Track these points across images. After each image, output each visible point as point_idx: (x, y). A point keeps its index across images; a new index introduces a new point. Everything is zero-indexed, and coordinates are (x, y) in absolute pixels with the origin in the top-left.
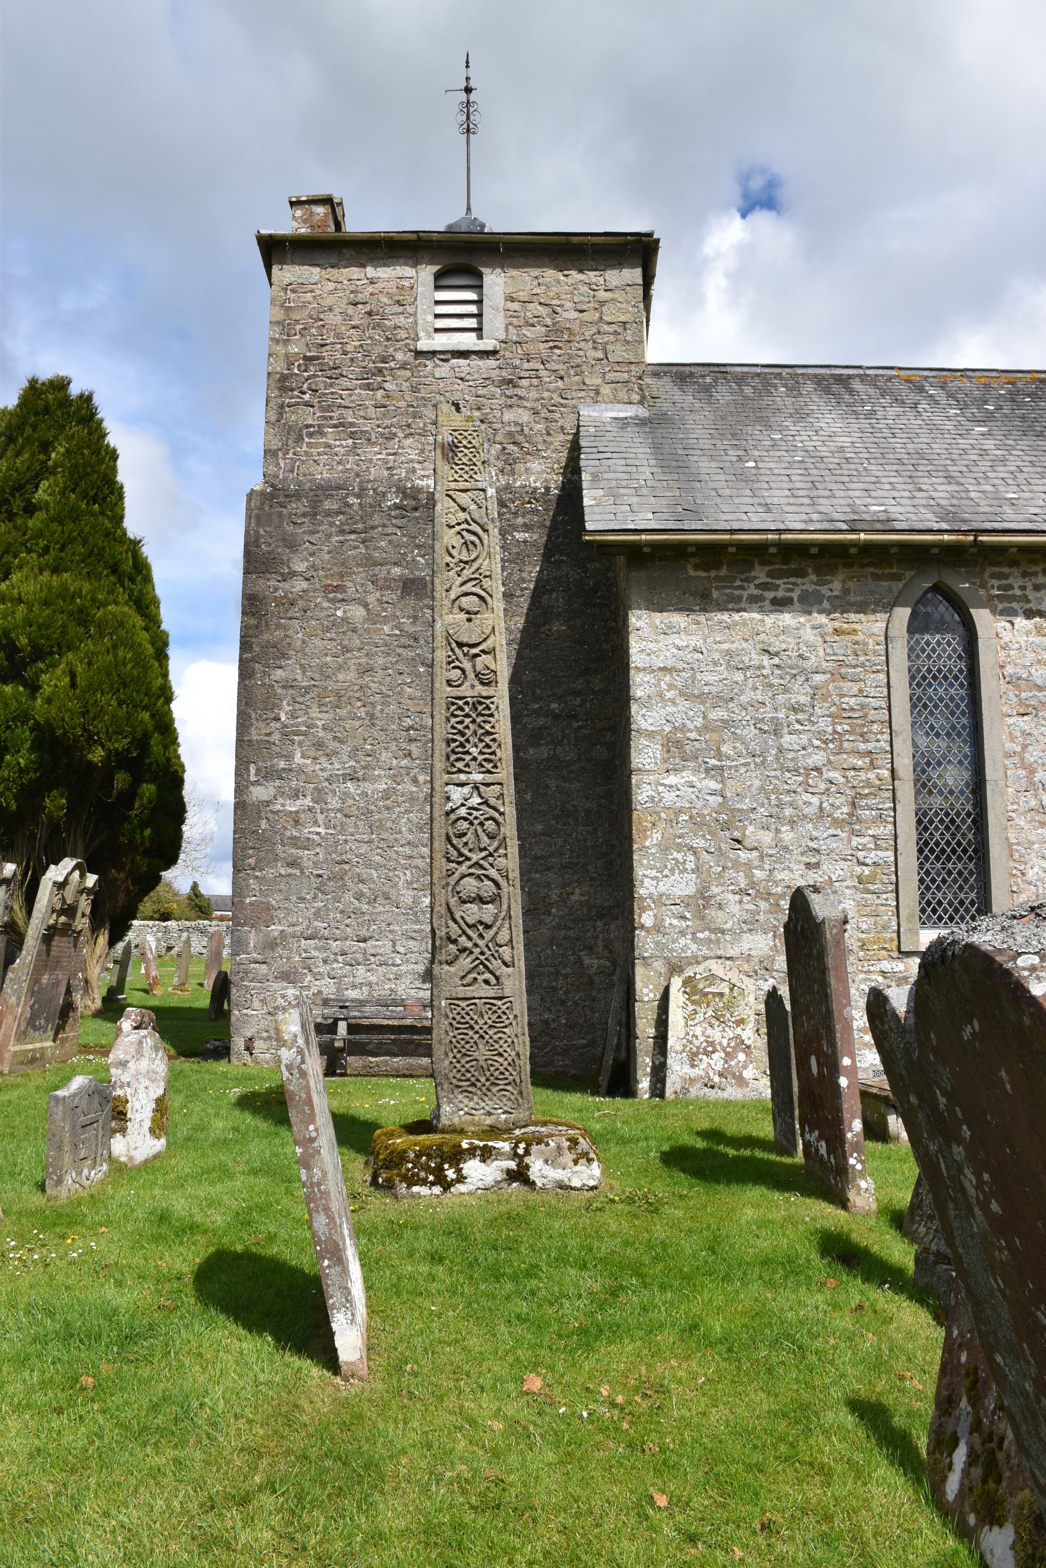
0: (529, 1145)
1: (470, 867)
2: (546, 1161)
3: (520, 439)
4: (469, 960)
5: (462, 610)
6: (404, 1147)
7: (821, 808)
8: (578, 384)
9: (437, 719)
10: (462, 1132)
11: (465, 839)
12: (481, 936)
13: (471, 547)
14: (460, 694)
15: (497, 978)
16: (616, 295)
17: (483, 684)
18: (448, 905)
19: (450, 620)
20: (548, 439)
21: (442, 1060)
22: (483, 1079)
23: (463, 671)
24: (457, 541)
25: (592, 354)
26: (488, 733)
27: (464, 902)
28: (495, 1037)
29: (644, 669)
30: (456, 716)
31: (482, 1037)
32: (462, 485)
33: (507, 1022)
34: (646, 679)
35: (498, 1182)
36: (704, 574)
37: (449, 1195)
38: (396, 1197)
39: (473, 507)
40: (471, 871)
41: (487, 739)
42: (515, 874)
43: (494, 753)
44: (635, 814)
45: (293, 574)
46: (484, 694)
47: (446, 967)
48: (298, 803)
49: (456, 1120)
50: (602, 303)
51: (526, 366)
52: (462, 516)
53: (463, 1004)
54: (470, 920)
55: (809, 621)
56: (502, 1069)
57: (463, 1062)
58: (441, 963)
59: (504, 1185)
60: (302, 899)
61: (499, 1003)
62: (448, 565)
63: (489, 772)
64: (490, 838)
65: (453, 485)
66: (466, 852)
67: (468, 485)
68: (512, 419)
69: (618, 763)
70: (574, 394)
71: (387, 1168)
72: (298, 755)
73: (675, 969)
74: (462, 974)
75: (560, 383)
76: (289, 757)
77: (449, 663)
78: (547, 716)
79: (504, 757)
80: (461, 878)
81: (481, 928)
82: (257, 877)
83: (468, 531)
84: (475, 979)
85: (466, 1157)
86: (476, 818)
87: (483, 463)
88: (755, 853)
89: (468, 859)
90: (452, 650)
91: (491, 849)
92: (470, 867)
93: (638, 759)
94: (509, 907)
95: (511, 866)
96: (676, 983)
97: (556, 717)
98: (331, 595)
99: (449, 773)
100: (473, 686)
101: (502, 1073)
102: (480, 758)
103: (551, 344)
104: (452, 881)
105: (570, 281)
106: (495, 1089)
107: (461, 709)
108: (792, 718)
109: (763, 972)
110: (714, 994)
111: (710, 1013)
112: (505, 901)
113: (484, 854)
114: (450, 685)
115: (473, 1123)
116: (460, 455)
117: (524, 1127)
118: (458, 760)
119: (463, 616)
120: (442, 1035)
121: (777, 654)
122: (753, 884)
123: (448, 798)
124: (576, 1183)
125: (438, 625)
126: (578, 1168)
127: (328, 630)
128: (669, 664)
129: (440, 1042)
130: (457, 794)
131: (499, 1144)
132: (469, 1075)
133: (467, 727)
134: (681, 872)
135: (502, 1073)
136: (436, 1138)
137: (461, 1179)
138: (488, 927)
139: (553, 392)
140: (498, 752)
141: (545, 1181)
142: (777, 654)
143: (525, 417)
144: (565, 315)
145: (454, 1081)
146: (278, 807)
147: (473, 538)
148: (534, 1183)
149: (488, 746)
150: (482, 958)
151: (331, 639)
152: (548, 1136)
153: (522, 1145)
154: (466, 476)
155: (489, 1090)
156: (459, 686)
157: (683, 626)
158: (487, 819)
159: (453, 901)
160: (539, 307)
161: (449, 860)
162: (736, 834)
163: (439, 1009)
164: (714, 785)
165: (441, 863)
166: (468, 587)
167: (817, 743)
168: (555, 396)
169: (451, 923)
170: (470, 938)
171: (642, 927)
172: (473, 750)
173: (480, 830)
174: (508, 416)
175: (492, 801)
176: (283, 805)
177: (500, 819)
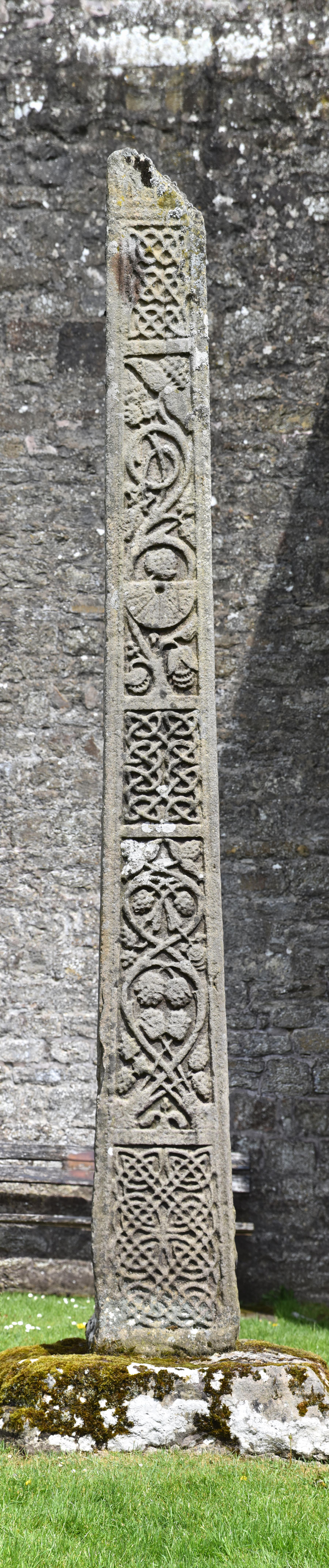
0: (228, 1376)
1: (154, 957)
2: (256, 1405)
4: (150, 1089)
5: (149, 573)
6: (42, 1368)
9: (111, 740)
10: (131, 1353)
11: (147, 917)
12: (167, 1055)
13: (165, 463)
14: (144, 706)
15: (189, 1117)
17: (178, 689)
18: (121, 1009)
19: (131, 589)
21: (107, 1238)
22: (165, 1271)
23: (150, 671)
24: (143, 454)
26: (184, 764)
27: (145, 1006)
28: (185, 1206)
30: (139, 738)
31: (165, 1205)
32: (153, 346)
33: (202, 1184)
34: (27, 1054)
35: (181, 1436)
37: (104, 1452)
38: (23, 1453)
39: (170, 388)
40: (156, 962)
41: (183, 773)
42: (217, 968)
43: (191, 794)
46: (180, 705)
47: (117, 1099)
49: (123, 1334)
52: (152, 405)
53: (139, 1154)
54: (153, 1033)
56: (193, 1255)
57: (136, 1241)
58: (109, 1093)
59: (190, 1441)
61: (191, 1154)
62: (128, 495)
63: (184, 821)
64: (183, 916)
65: (137, 346)
66: (148, 934)
67: (160, 346)
71: (13, 1403)
77: (130, 658)
79: (205, 800)
80: (142, 972)
81: (167, 1043)
83: (161, 433)
84: (157, 1118)
85: (134, 1389)
86: (164, 887)
87: (190, 297)
89: (152, 945)
90: (134, 638)
91: (184, 931)
92: (154, 957)
94: (208, 1015)
95: (211, 956)
99: (127, 822)
100: (163, 694)
101: (193, 1262)
102: (172, 800)
104: (129, 975)
106: (182, 1287)
112: (202, 1005)
113: (174, 938)
114: (130, 692)
115: (148, 1340)
116: (149, 281)
117: (226, 1350)
119: (151, 583)
120: (106, 1199)
123: (125, 859)
124: (304, 1446)
125: (113, 598)
126: (305, 1420)
129: (104, 1210)
130: (138, 853)
131: (184, 1373)
132: (144, 1263)
133: (154, 755)
135: (193, 1262)
136: (91, 1359)
137: (124, 1426)
138: (177, 1042)
140: (197, 791)
141: (254, 1439)
145: (123, 1271)
147: (169, 447)
148: (236, 1442)
149: (183, 783)
150: (168, 1087)
152: (259, 1365)
153: (219, 1376)
154: (159, 327)
155: (173, 1287)
156: (144, 693)
158: (179, 889)
159: (129, 1005)
161: (124, 946)
163: (105, 1159)
165: (114, 951)
169: (125, 1036)
170: (151, 1058)
175: (188, 864)
177: (198, 889)
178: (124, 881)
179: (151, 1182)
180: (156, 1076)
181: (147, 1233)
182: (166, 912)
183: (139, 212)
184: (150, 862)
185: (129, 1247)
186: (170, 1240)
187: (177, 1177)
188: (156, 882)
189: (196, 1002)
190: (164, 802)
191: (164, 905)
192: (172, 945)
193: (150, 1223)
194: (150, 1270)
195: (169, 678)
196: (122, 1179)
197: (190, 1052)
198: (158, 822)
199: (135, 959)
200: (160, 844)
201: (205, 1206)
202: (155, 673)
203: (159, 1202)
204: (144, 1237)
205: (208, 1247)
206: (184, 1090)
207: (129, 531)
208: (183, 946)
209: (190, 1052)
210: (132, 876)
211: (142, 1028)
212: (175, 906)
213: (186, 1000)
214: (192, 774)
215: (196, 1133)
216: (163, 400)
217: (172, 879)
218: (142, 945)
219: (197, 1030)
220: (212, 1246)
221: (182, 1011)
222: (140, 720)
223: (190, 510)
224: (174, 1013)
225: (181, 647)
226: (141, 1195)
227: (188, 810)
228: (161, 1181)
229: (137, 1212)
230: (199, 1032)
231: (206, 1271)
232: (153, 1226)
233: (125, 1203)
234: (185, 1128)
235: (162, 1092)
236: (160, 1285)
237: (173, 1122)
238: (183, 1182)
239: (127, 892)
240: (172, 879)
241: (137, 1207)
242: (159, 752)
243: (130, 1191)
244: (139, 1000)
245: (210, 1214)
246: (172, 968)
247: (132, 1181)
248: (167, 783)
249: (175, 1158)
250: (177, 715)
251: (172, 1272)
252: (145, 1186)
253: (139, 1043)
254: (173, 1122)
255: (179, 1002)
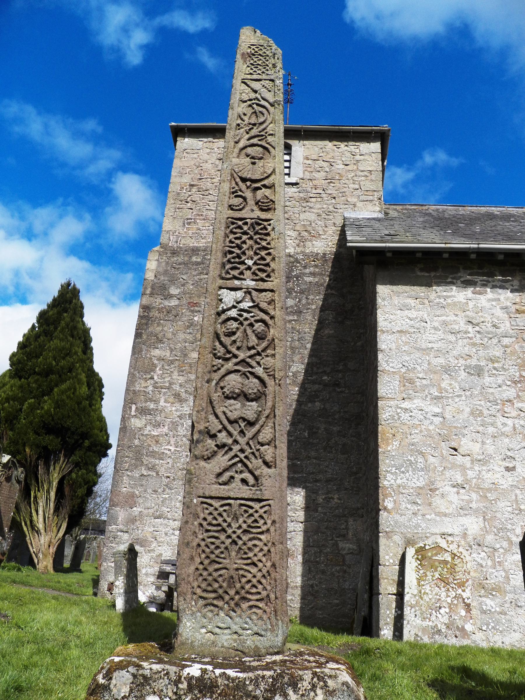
1: (236, 364)
3: (309, 228)
4: (227, 457)
5: (248, 156)
7: (514, 428)
8: (343, 201)
11: (233, 338)
15: (256, 478)
16: (366, 157)
17: (262, 210)
20: (326, 229)
23: (245, 199)
25: (352, 186)
27: (228, 398)
28: (250, 544)
29: (388, 331)
30: (235, 233)
32: (255, 77)
33: (264, 528)
36: (427, 274)
41: (263, 253)
44: (380, 428)
45: (171, 296)
47: (202, 463)
48: (159, 430)
50: (358, 161)
51: (314, 191)
52: (253, 95)
53: (216, 504)
54: (233, 416)
55: (499, 304)
57: (211, 569)
60: (155, 491)
61: (257, 506)
66: (234, 350)
67: (259, 77)
68: (305, 218)
69: (364, 414)
70: (342, 206)
72: (162, 400)
73: (409, 543)
74: (218, 471)
75: (333, 201)
76: (157, 402)
78: (320, 384)
81: (243, 425)
82: (128, 475)
84: (232, 477)
86: (246, 319)
88: (468, 458)
89: (235, 356)
90: (237, 184)
91: (260, 349)
92: (236, 364)
93: (382, 390)
94: (274, 406)
96: (411, 552)
97: (326, 385)
98: (192, 309)
99: (223, 278)
102: (254, 268)
103: (329, 181)
105: (340, 150)
106: (245, 605)
107: (240, 227)
108: (491, 365)
109: (476, 547)
110: (440, 562)
111: (437, 575)
112: (270, 398)
113: (253, 352)
114: (232, 209)
118: (232, 269)
121: (477, 325)
122: (467, 481)
127: (188, 327)
128: (404, 328)
130: (229, 297)
132: (216, 585)
134: (414, 470)
138: (251, 424)
139: (329, 205)
142: (477, 325)
143: (313, 217)
144: (337, 167)
145: (199, 591)
146: (146, 432)
149: (263, 259)
150: (242, 456)
151: (190, 333)
156: (240, 210)
157: (413, 305)
158: (257, 321)
159: (216, 396)
160: (322, 163)
162: (454, 444)
164: (437, 410)
166: (255, 141)
167: (509, 383)
168: (330, 207)
169: (212, 418)
170: (230, 434)
171: (385, 509)
172: (250, 262)
173: (249, 331)
174: (303, 216)
175: (264, 305)
176: (150, 431)
177: (270, 322)
178: (219, 314)
179: (225, 525)
180: (232, 447)
181: (220, 563)
182: (247, 335)
183: (252, 41)
184: (238, 303)
185: (205, 573)
186: (237, 569)
187: (245, 522)
188: (241, 316)
189: (266, 396)
190: (249, 268)
191: (245, 330)
192: (250, 357)
193: (223, 556)
194: (221, 591)
195: (257, 203)
196: (202, 522)
197: (259, 431)
198: (245, 280)
199: (222, 366)
200: (245, 292)
201: (265, 545)
202: (248, 200)
203: (230, 540)
204: (217, 566)
205: (266, 575)
206: (253, 458)
207: (238, 138)
208: (258, 358)
209: (259, 431)
210: (224, 311)
211: (224, 413)
212: (253, 331)
213: (258, 394)
214: (269, 254)
215: (261, 490)
216: (260, 94)
217: (252, 314)
218: (228, 356)
219: (265, 416)
220: (269, 575)
221: (254, 403)
222: (237, 223)
223: (271, 132)
224: (248, 403)
225: (264, 189)
226: (216, 534)
227: (265, 274)
228: (232, 524)
229: (213, 547)
230: (267, 417)
231: (264, 593)
232: (224, 558)
233: (203, 540)
234: (253, 486)
235: (238, 459)
236: (227, 603)
237: (244, 481)
238: (249, 526)
239: (220, 321)
240: (252, 314)
241: (213, 543)
242: (247, 241)
243: (207, 531)
244: (223, 393)
245: (269, 551)
246: (249, 372)
247: (210, 524)
248: (252, 259)
249: (244, 508)
250: (260, 222)
251: (237, 593)
252: (220, 528)
253: (221, 423)
254: (244, 481)
255: (253, 396)
